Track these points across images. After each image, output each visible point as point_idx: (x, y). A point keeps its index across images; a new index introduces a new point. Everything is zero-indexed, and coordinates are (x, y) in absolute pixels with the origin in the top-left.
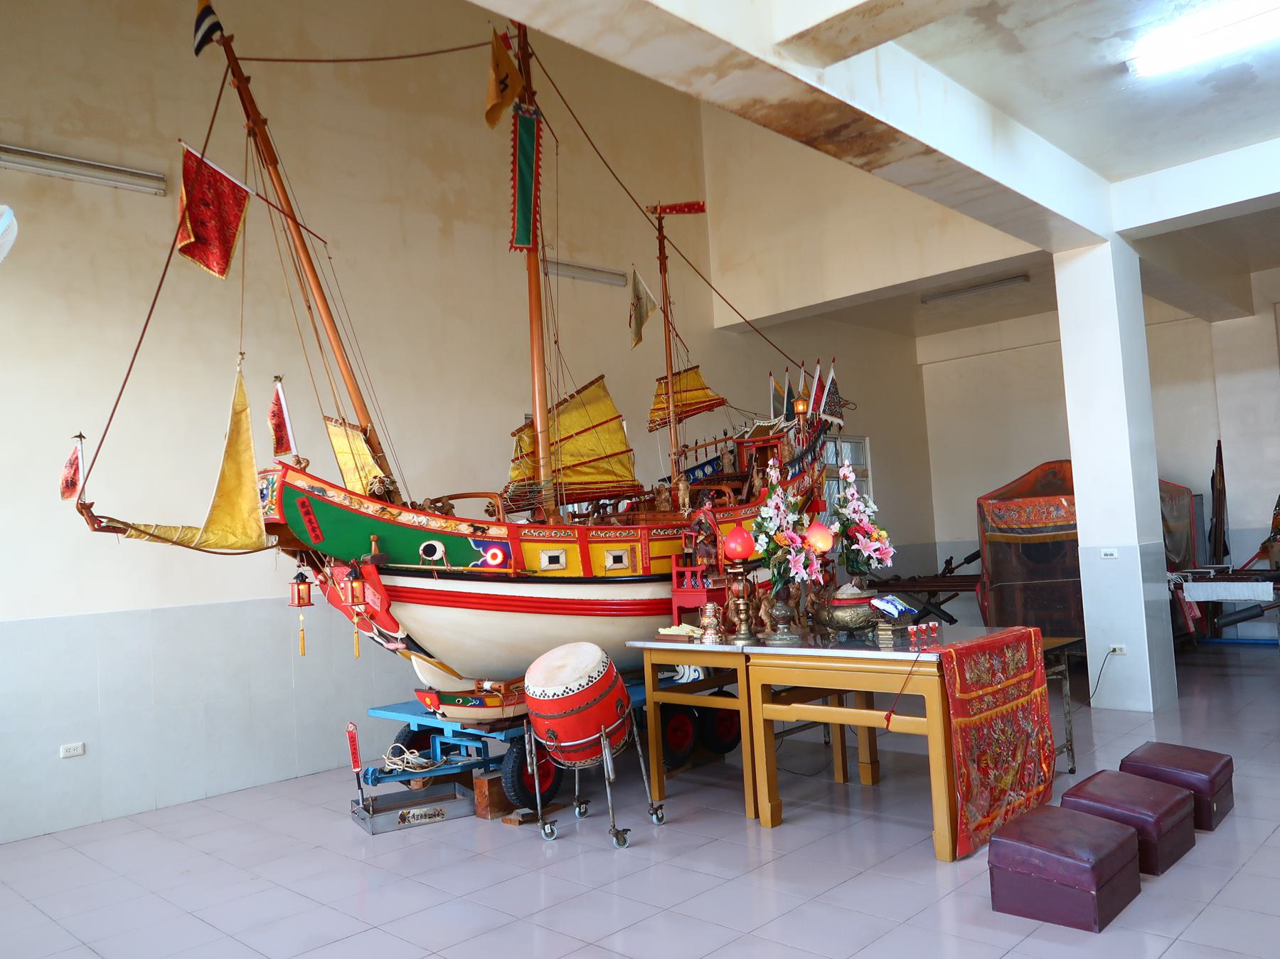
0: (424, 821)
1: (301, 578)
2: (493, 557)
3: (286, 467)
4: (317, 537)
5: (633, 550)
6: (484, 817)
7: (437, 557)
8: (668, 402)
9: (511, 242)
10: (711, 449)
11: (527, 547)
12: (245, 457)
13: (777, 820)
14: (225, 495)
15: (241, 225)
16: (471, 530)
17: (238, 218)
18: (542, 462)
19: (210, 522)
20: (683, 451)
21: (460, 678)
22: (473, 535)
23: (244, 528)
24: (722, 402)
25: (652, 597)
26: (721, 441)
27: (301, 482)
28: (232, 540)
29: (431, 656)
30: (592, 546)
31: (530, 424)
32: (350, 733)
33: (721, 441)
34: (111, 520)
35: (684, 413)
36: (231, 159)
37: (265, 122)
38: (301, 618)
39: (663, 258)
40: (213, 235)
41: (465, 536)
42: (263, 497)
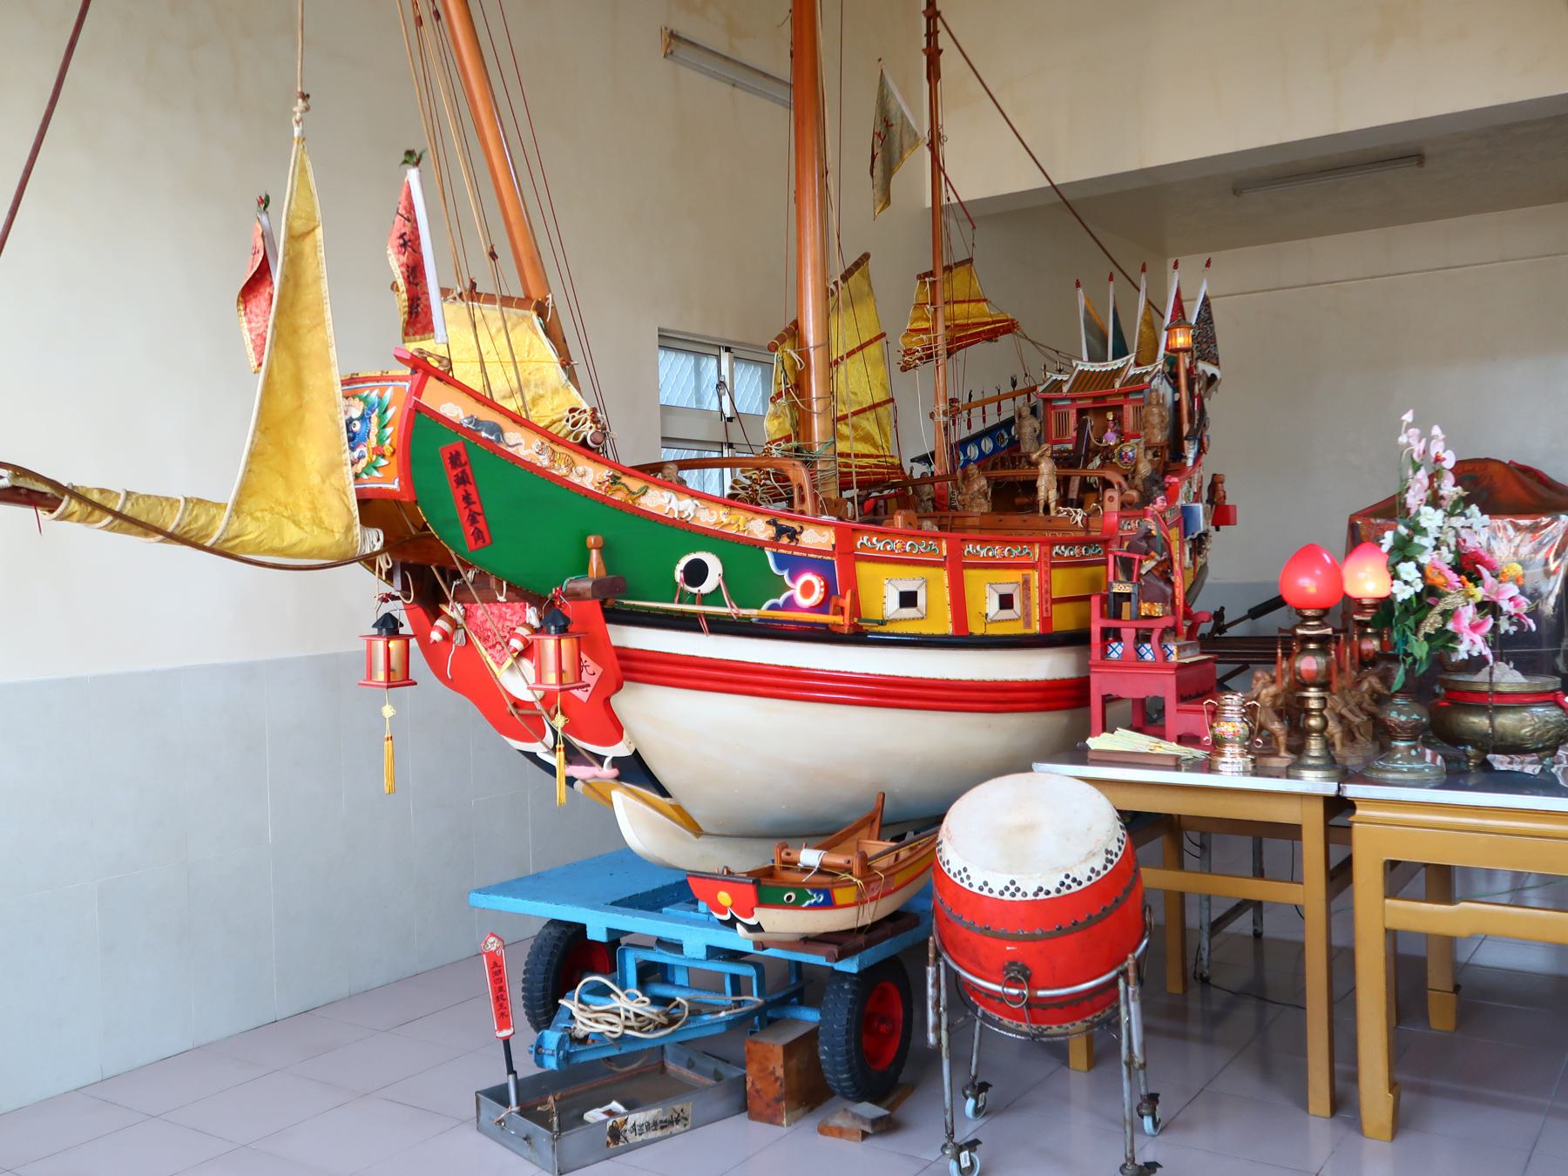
0: (652, 1135)
1: (388, 626)
2: (805, 591)
4: (479, 536)
6: (772, 1120)
7: (707, 587)
8: (935, 319)
10: (991, 408)
11: (863, 569)
12: (311, 343)
13: (1400, 1123)
14: (274, 430)
16: (770, 532)
18: (815, 408)
19: (245, 491)
20: (953, 408)
21: (697, 831)
22: (774, 542)
23: (314, 509)
24: (1009, 327)
25: (1050, 677)
26: (1006, 396)
27: (454, 409)
28: (292, 534)
29: (664, 793)
30: (969, 574)
31: (794, 332)
32: (491, 955)
33: (1006, 396)
34: (19, 471)
38: (388, 711)
39: (933, 54)
41: (759, 545)
42: (353, 440)
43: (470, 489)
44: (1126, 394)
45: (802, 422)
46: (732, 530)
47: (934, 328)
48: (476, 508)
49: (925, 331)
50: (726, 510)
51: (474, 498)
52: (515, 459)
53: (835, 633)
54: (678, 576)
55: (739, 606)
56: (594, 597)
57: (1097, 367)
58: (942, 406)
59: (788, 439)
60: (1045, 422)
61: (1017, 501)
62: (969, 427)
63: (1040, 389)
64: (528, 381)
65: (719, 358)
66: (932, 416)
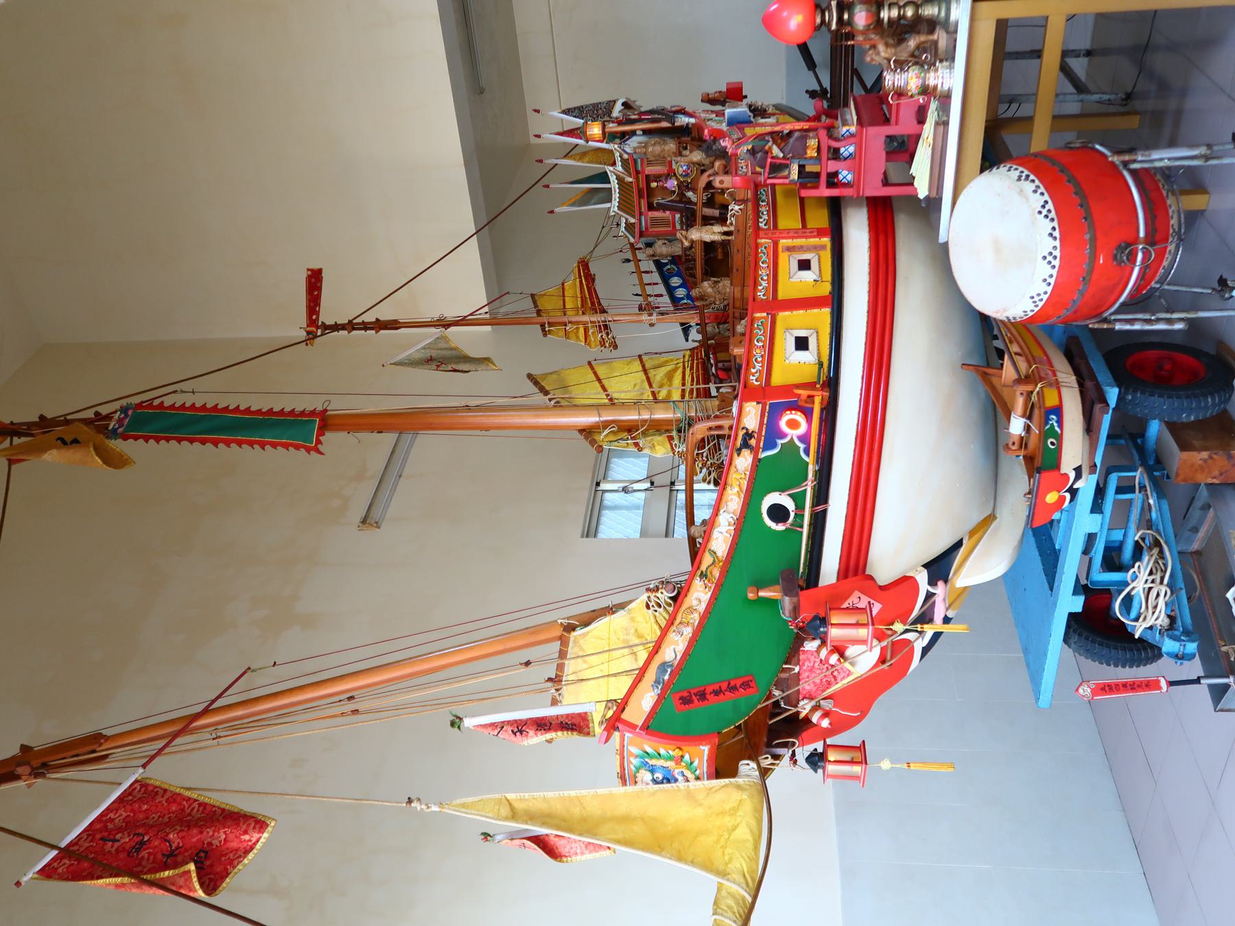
1: (816, 760)
2: (796, 427)
3: (613, 724)
4: (747, 684)
5: (790, 249)
7: (790, 505)
8: (578, 323)
9: (308, 450)
10: (647, 278)
11: (777, 379)
14: (660, 841)
15: (188, 794)
17: (175, 798)
18: (646, 416)
19: (708, 867)
21: (990, 519)
22: (754, 451)
23: (723, 813)
24: (584, 265)
25: (866, 229)
26: (638, 267)
27: (646, 700)
28: (743, 834)
29: (959, 544)
30: (781, 295)
31: (587, 432)
33: (638, 267)
35: (592, 303)
36: (79, 804)
37: (25, 749)
39: (380, 325)
40: (195, 837)
41: (757, 463)
42: (668, 780)
43: (709, 690)
44: (637, 172)
45: (657, 427)
46: (745, 483)
47: (585, 323)
48: (724, 686)
49: (586, 330)
50: (728, 489)
51: (717, 687)
52: (686, 653)
53: (829, 403)
54: (780, 527)
55: (806, 479)
56: (797, 595)
57: (616, 196)
58: (645, 317)
59: (671, 438)
60: (659, 236)
61: (720, 257)
62: (661, 296)
63: (632, 240)
64: (624, 641)
65: (604, 491)
66: (652, 325)
